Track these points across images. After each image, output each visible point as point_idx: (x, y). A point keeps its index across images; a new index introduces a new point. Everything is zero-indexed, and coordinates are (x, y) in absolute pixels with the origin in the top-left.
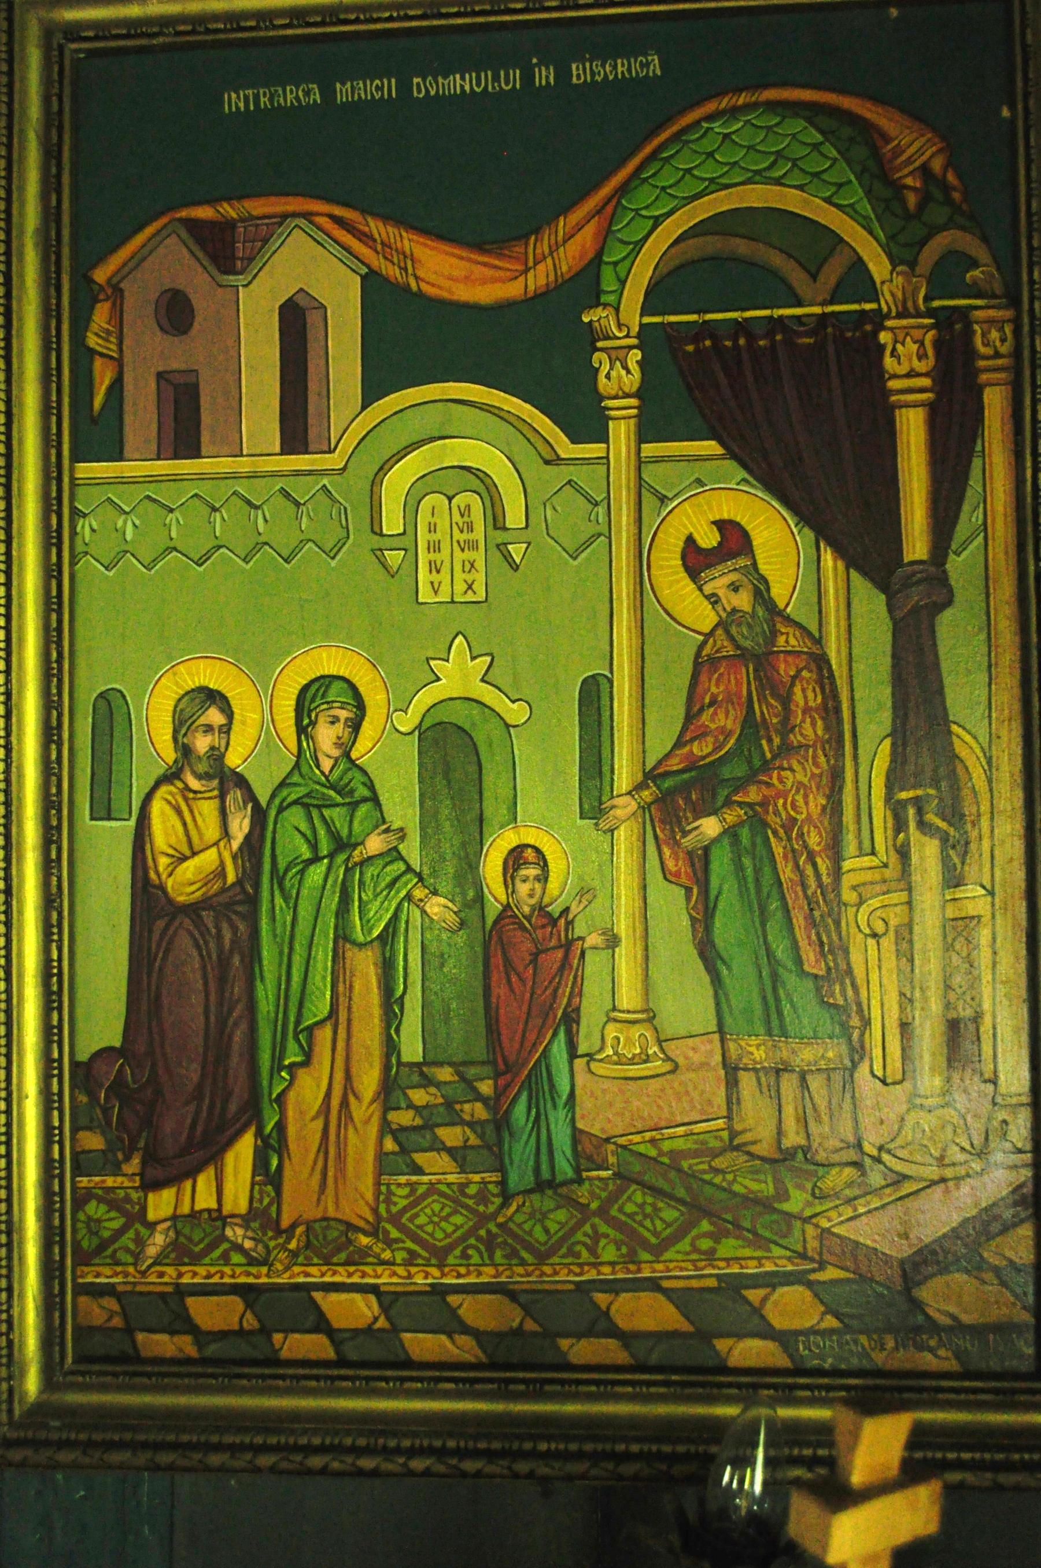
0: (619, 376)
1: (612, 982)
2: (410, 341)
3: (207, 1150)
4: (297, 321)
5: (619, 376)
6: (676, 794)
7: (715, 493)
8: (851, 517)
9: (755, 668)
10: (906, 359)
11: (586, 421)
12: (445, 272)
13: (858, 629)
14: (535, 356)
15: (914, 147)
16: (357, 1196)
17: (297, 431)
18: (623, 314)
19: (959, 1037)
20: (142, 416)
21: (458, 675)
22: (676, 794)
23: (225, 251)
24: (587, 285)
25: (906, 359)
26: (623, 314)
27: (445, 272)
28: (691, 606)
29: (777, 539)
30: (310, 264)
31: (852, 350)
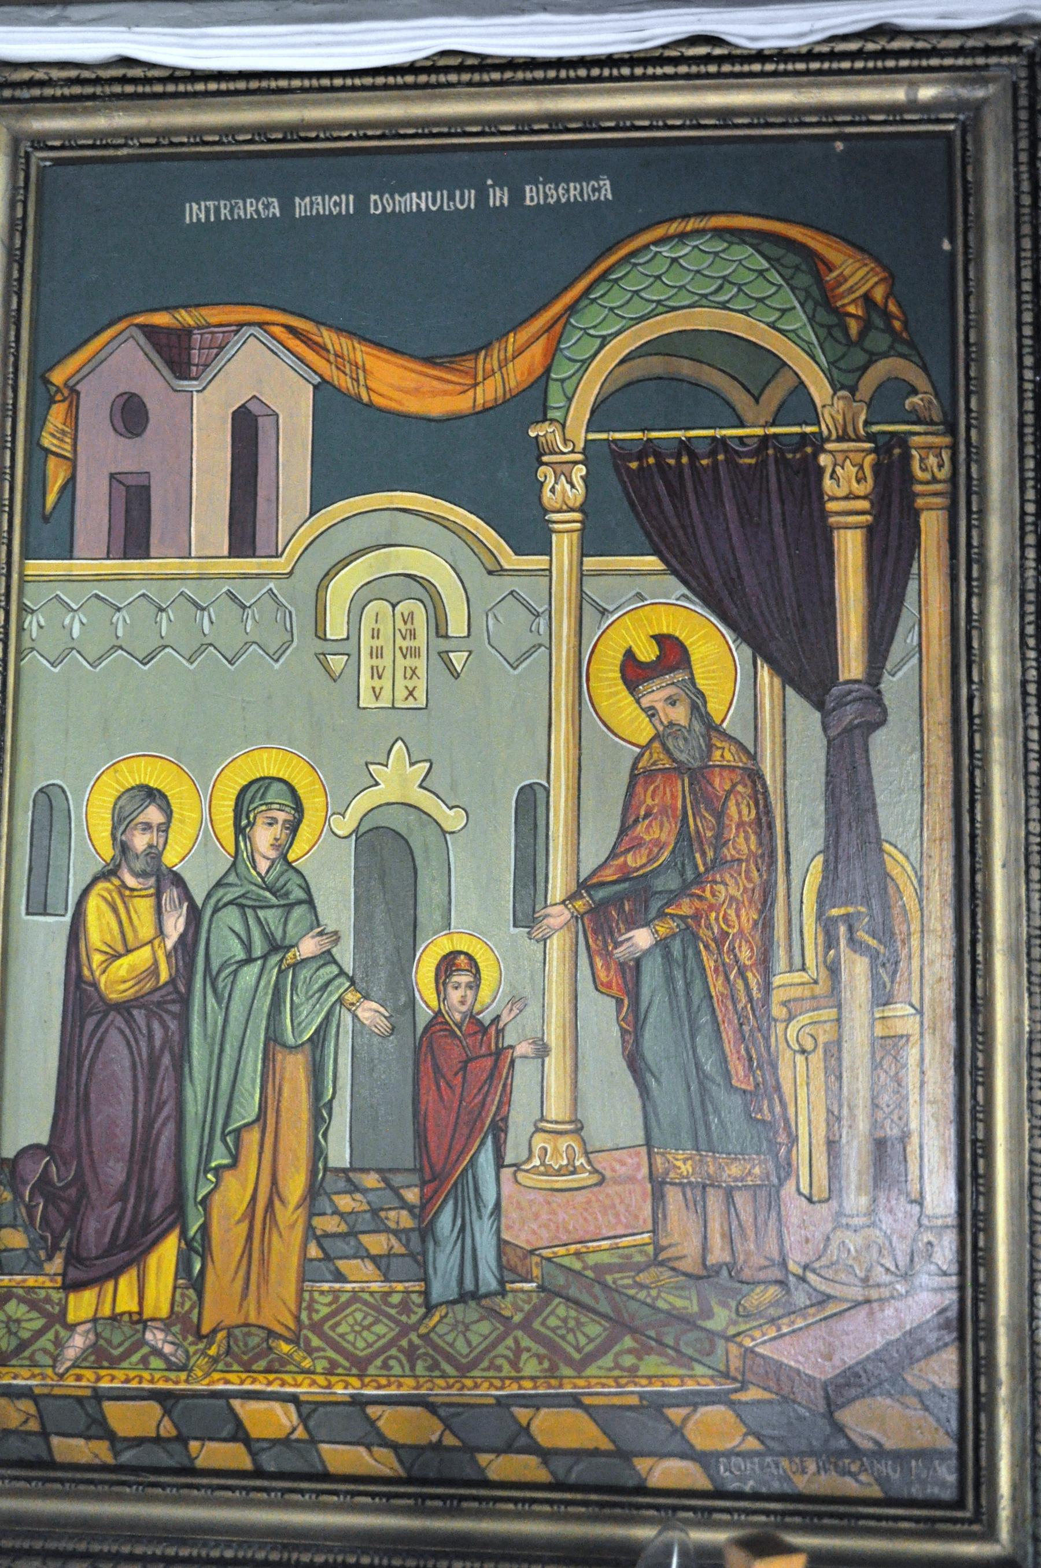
0: (564, 490)
1: (541, 1091)
2: (358, 448)
3: (130, 1249)
4: (247, 427)
5: (564, 490)
6: (609, 904)
7: (654, 604)
8: (790, 639)
9: (690, 778)
10: (846, 482)
11: (530, 533)
12: (394, 382)
13: (792, 744)
14: (482, 468)
15: (855, 275)
16: (277, 1307)
17: (244, 536)
18: (570, 428)
19: (886, 1155)
20: (94, 513)
21: (397, 780)
22: (609, 904)
23: (177, 354)
24: (535, 400)
25: (846, 482)
26: (570, 428)
27: (394, 382)
28: (629, 718)
29: (714, 651)
30: (264, 371)
31: (794, 469)
